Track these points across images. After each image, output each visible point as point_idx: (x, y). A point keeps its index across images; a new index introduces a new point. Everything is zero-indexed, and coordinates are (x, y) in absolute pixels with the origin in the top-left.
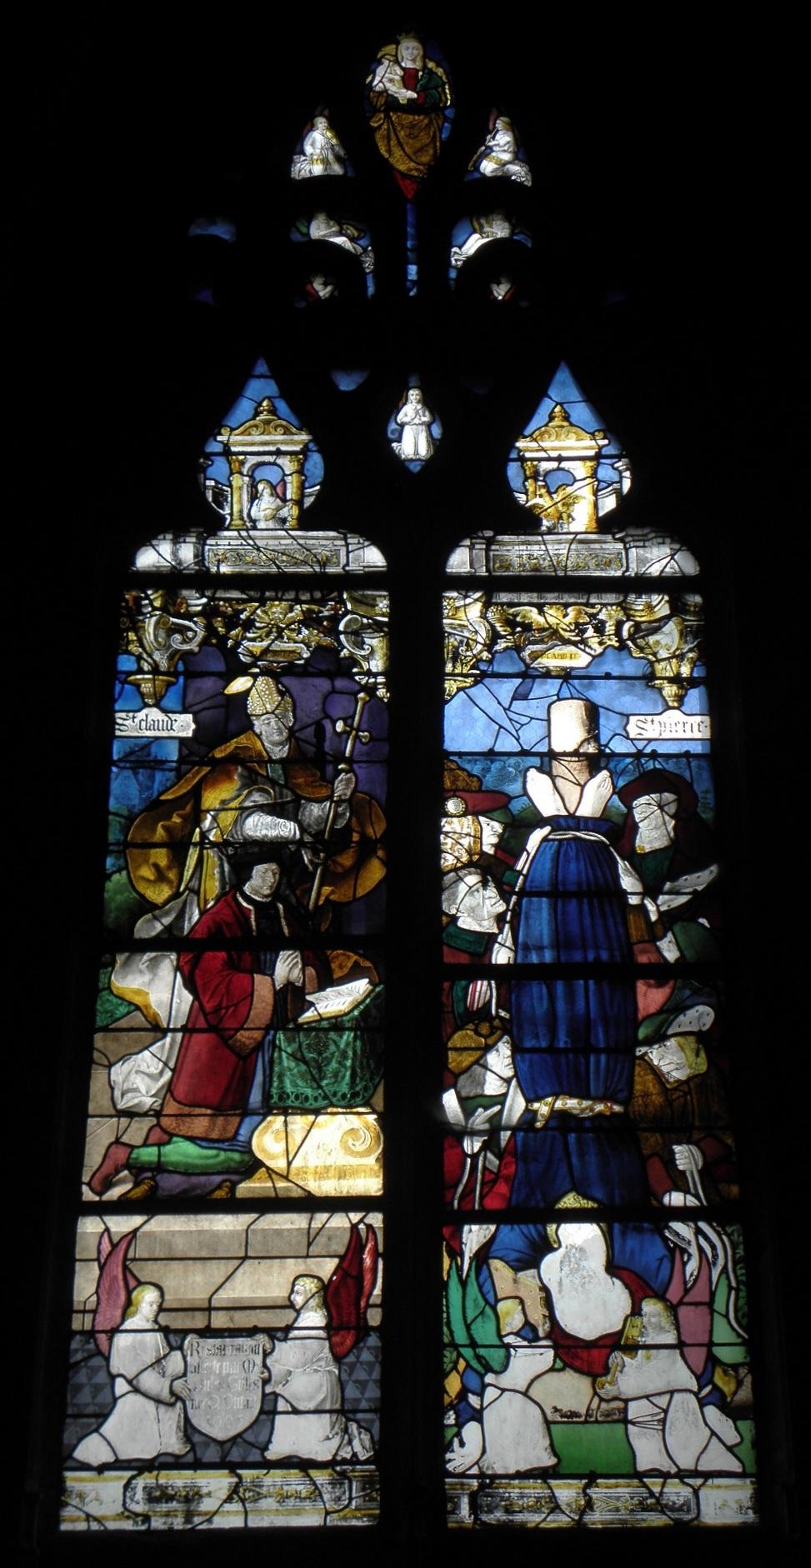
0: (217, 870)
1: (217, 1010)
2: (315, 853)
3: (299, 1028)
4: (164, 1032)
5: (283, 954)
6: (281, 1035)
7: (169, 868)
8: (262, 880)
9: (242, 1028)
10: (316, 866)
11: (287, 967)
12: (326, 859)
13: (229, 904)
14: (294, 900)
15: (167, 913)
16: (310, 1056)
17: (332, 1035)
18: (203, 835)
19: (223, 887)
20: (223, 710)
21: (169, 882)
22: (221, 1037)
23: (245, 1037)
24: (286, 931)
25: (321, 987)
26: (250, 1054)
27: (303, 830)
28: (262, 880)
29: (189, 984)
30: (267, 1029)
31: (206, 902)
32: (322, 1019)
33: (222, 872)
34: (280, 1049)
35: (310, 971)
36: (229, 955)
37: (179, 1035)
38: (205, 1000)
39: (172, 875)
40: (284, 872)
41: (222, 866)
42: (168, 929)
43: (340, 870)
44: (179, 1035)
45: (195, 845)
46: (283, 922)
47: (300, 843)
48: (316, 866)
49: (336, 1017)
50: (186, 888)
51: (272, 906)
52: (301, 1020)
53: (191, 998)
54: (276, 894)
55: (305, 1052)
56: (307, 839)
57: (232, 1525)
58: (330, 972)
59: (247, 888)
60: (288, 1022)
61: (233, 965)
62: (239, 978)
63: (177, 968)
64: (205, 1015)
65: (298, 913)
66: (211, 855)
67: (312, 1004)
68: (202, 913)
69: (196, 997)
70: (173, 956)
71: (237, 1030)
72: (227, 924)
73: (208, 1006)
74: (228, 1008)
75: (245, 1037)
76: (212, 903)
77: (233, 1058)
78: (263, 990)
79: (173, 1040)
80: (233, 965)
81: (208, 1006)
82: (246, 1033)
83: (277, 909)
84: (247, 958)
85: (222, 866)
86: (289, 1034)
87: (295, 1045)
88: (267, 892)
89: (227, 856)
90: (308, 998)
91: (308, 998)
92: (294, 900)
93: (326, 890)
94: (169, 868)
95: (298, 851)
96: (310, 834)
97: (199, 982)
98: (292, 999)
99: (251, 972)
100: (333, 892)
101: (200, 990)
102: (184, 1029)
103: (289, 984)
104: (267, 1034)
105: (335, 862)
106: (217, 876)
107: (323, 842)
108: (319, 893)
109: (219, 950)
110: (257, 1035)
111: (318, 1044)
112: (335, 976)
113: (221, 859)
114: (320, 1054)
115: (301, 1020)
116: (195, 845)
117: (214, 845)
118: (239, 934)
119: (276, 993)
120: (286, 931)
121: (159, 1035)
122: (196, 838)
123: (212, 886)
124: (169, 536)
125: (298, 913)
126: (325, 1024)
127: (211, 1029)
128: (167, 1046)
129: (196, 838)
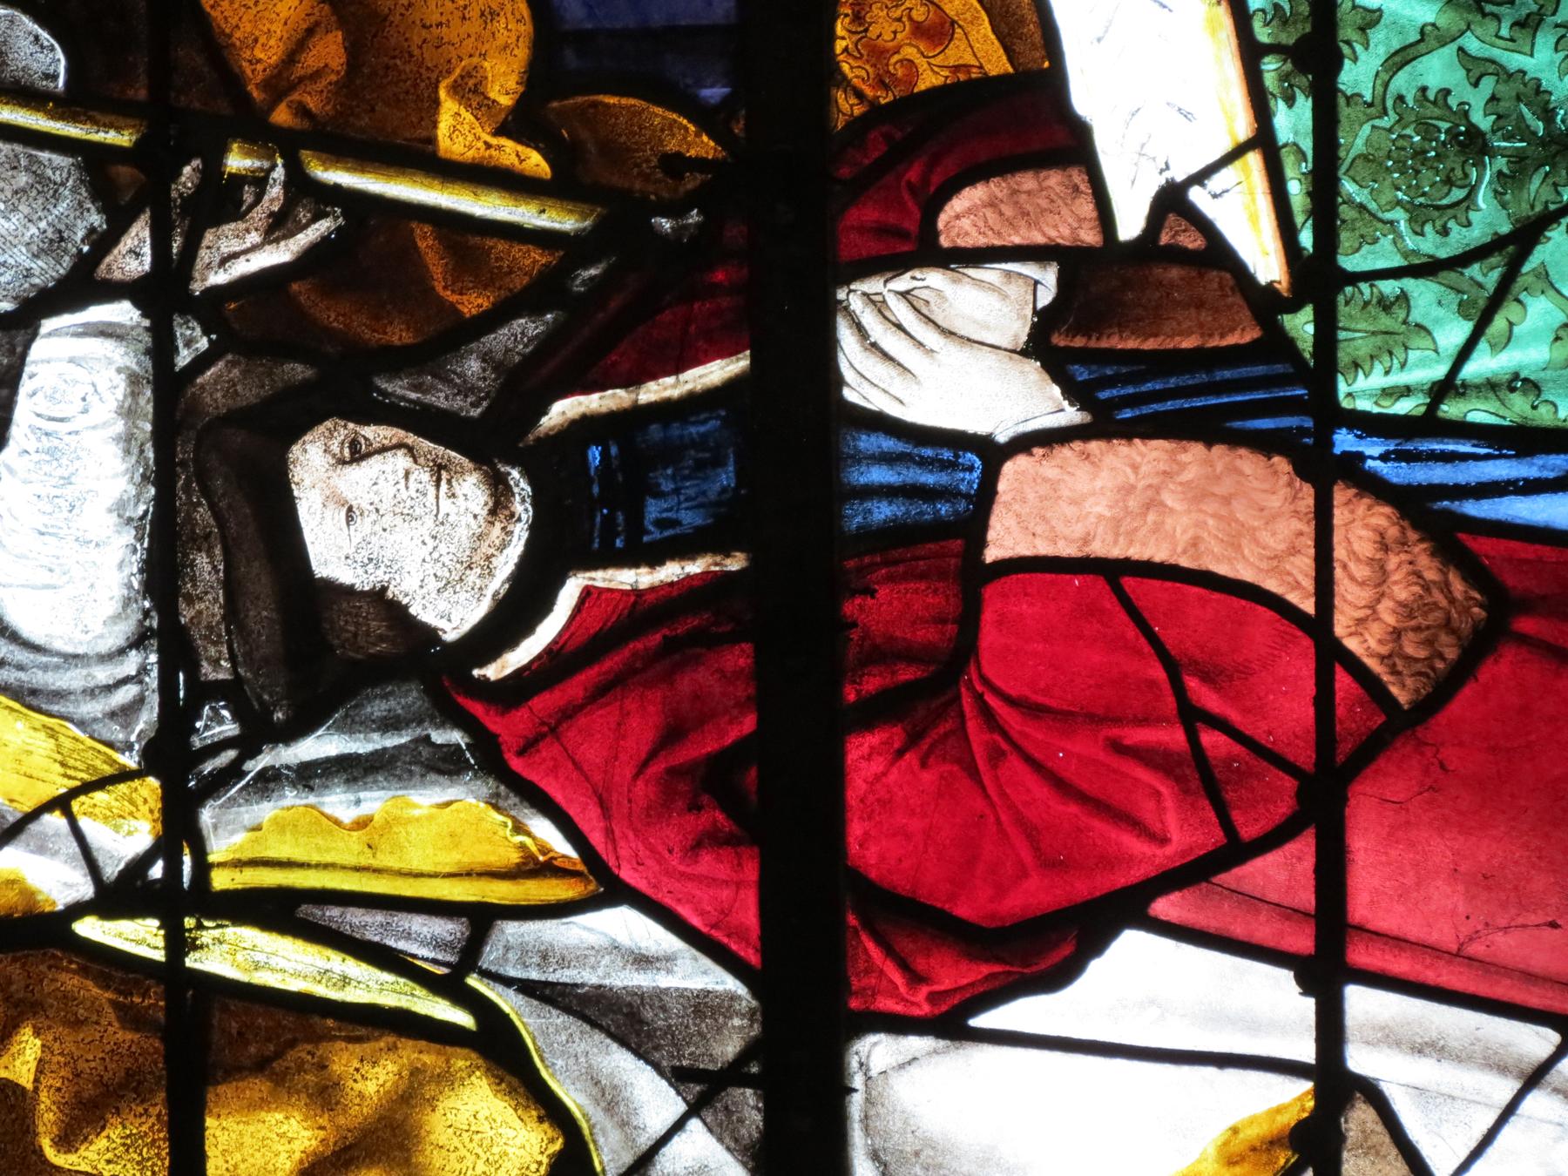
0: (338, 802)
1: (1207, 783)
2: (222, 201)
3: (1317, 277)
4: (1335, 1084)
5: (865, 381)
6: (1360, 390)
7: (326, 1096)
8: (399, 526)
9: (1319, 626)
10: (307, 195)
11: (940, 354)
12: (260, 135)
13: (551, 730)
14: (523, 331)
15: (611, 1099)
16: (1488, 217)
17: (1357, 76)
18: (120, 895)
19: (447, 765)
20: (75, 805)
21: (411, 1098)
22: (1371, 749)
23: (1379, 596)
24: (714, 373)
25: (1071, 147)
26: (1474, 572)
27: (80, 285)
28: (399, 526)
29: (1054, 947)
30: (1324, 472)
31: (537, 867)
32: (1264, 140)
33: (351, 770)
34: (1445, 388)
35: (965, 216)
36: (871, 714)
37: (1360, 1002)
38: (1146, 858)
39: (372, 1077)
40: (347, 391)
41: (309, 775)
42: (703, 1090)
43: (329, 52)
44: (1360, 1002)
45: (178, 943)
46: (1143, 389)
47: (163, 294)
48: (307, 195)
49: (1251, 53)
50: (450, 986)
51: (555, 464)
52: (1266, 263)
53: (1132, 949)
54: (485, 439)
55: (1461, 239)
56: (133, 256)
57: (1336, 546)
58: (969, 93)
59: (454, 614)
60: (1277, 344)
61: (932, 694)
62: (1009, 647)
63: (951, 1025)
64: (1236, 851)
65: (611, 307)
66: (235, 836)
67: (1171, 201)
68: (611, 892)
69: (1128, 908)
70: (876, 1053)
71: (1331, 654)
72: (672, 734)
73: (1184, 831)
74: (1191, 716)
75: (1379, 596)
76: (545, 831)
77: (1500, 668)
78: (1075, 504)
79: (1390, 1038)
80: (932, 694)
81: (1184, 831)
82: (1350, 596)
83: (586, 427)
84: (890, 608)
85: (309, 775)
86: (1354, 338)
87: (1424, 295)
88: (471, 491)
89: (248, 745)
90: (1130, 225)
91: (1130, 225)
92: (523, 331)
93: (457, 130)
94: (326, 1096)
95: (211, 308)
96: (103, 243)
97: (1036, 894)
98: (1147, 333)
99: (977, 576)
100: (471, 91)
101: (1082, 888)
102: (1324, 976)
103: (1045, 345)
104: (1352, 469)
105: (280, 83)
106: (375, 801)
107: (155, 160)
108: (477, 175)
109: (834, 775)
110: (1360, 526)
111: (1413, 161)
112: (997, 63)
113: (269, 781)
114: (1473, 144)
115: (1266, 263)
116: (178, 943)
117: (179, 827)
118: (739, 657)
119: (1104, 424)
120: (714, 373)
121: (1359, 1119)
122: (139, 937)
123: (443, 830)
124: (543, 1112)
125: (611, 307)
126: (1293, 122)
127: (1321, 811)
128: (1426, 1071)
129: (139, 937)
